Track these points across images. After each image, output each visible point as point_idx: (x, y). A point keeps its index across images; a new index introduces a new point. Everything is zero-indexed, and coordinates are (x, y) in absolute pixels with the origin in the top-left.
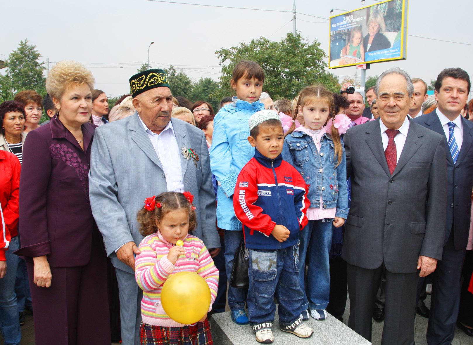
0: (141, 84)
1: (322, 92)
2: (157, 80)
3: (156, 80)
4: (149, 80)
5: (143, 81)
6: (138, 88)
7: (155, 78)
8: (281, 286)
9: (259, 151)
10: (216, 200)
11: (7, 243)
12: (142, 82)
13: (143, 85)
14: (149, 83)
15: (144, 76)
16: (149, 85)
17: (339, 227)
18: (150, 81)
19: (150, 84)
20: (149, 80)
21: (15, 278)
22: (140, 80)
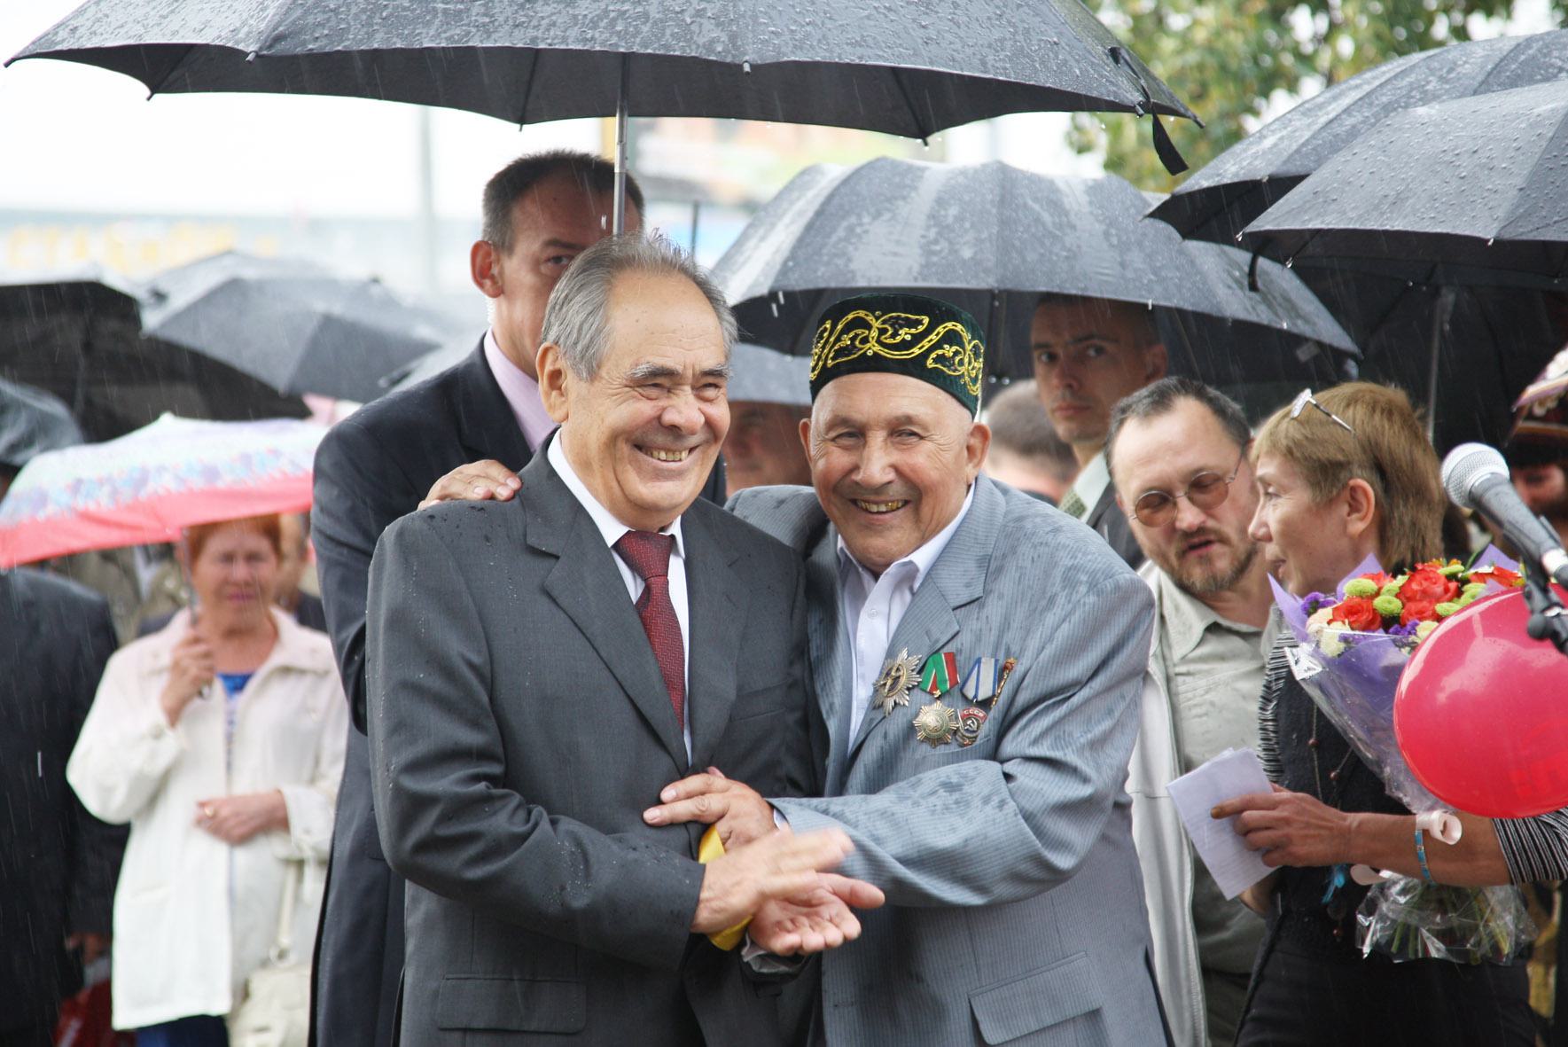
0: (851, 335)
1: (1221, 484)
2: (886, 331)
3: (857, 343)
4: (938, 345)
5: (913, 331)
6: (877, 348)
7: (888, 341)
8: (1400, 879)
9: (1203, 606)
10: (1366, 675)
11: (1332, 775)
12: (905, 334)
13: (905, 345)
14: (933, 355)
15: (926, 320)
16: (930, 363)
17: (779, 954)
18: (940, 352)
19: (935, 360)
20: (938, 345)
21: (1095, 1008)
22: (897, 324)
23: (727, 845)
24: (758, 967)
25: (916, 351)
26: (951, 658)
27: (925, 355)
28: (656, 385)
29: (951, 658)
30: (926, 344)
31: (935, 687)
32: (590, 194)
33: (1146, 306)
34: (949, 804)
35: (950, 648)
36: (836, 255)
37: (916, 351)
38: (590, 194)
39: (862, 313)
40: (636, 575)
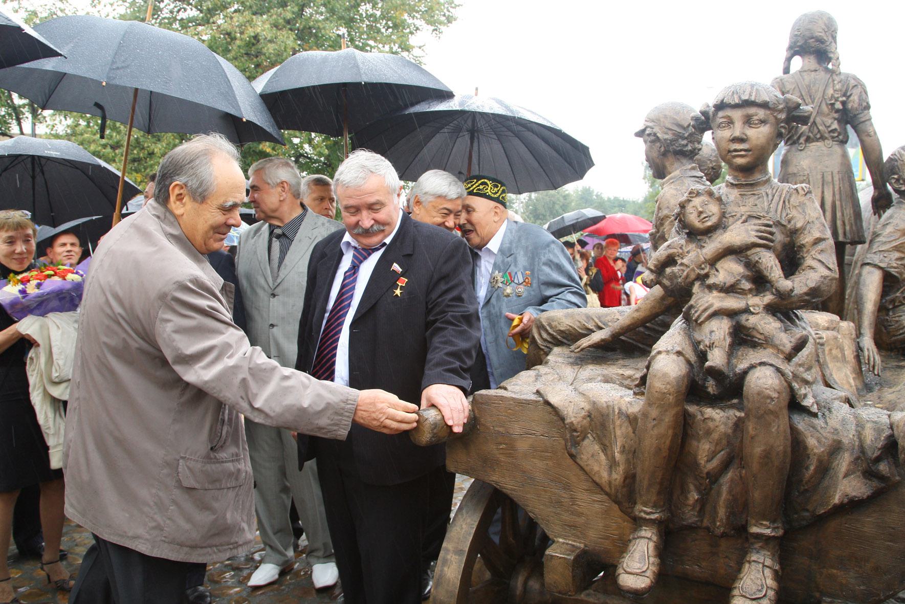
16: (475, 191)
20: (478, 186)
23: (638, 261)
24: (478, 398)
25: (471, 189)
26: (510, 274)
27: (473, 190)
28: (210, 546)
29: (510, 274)
30: (474, 186)
31: (507, 282)
32: (465, 359)
33: (361, 83)
34: (609, 257)
35: (509, 271)
36: (198, 22)
37: (471, 189)
38: (465, 359)
39: (486, 180)
40: (533, 368)
